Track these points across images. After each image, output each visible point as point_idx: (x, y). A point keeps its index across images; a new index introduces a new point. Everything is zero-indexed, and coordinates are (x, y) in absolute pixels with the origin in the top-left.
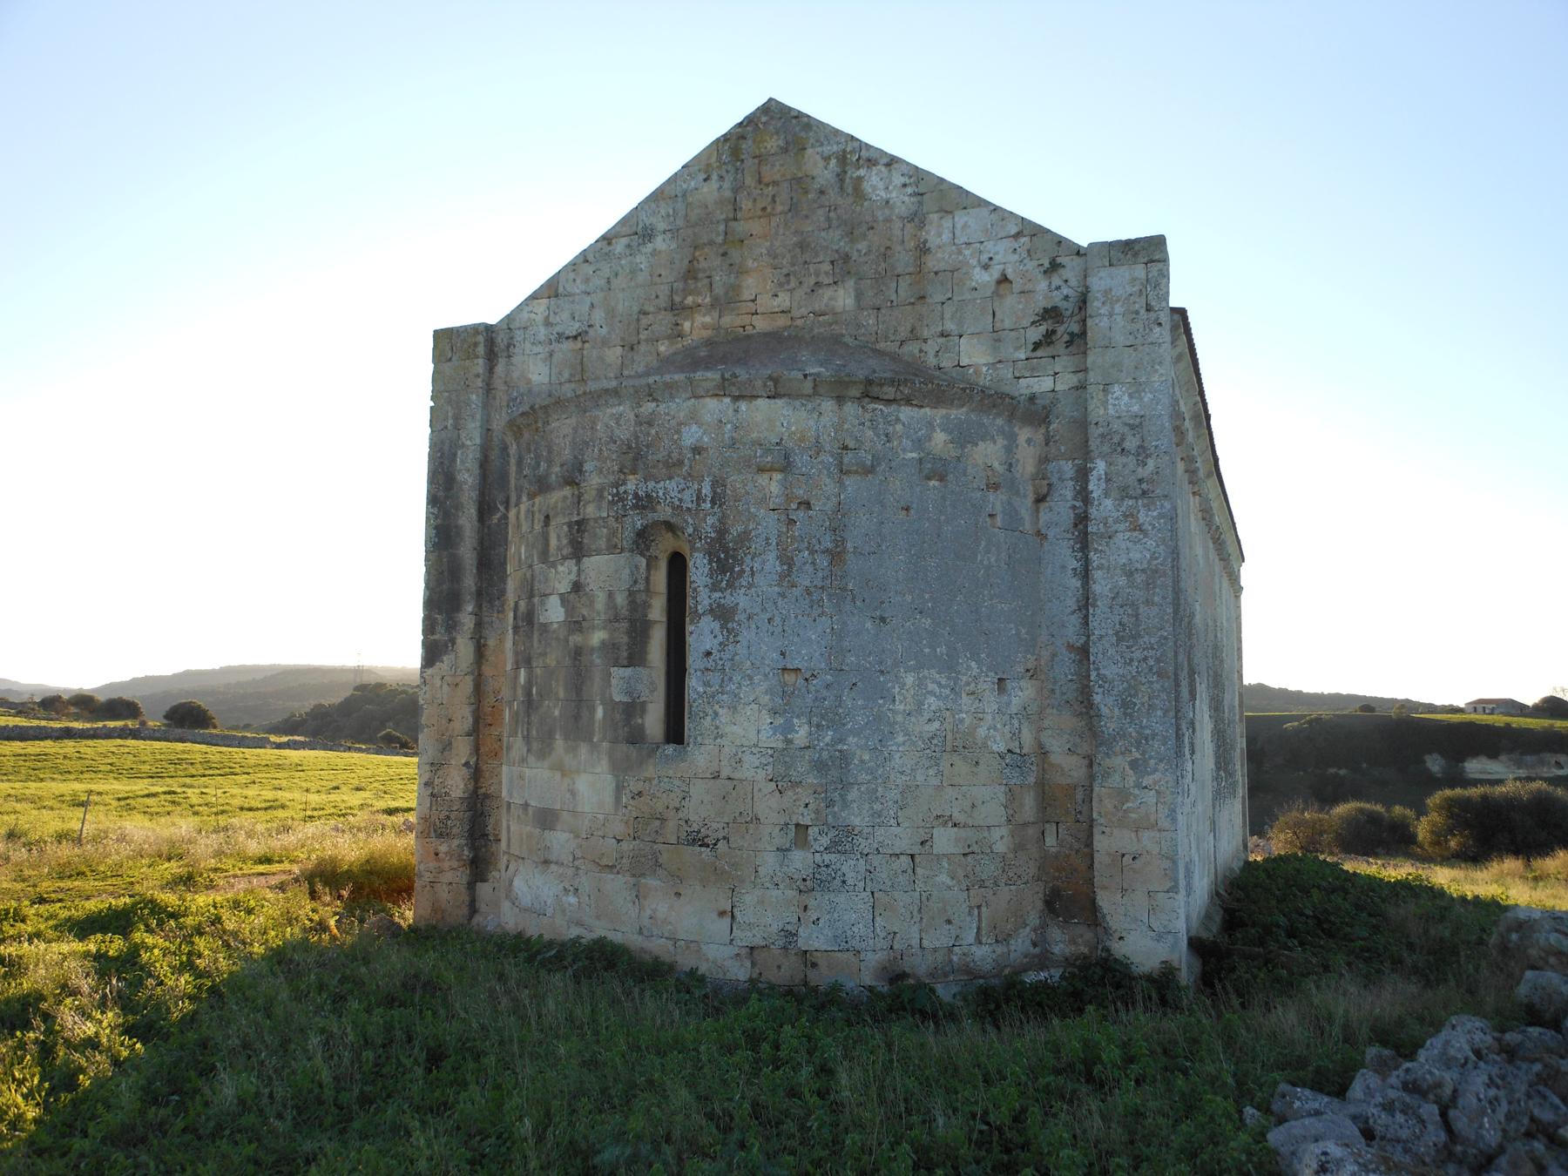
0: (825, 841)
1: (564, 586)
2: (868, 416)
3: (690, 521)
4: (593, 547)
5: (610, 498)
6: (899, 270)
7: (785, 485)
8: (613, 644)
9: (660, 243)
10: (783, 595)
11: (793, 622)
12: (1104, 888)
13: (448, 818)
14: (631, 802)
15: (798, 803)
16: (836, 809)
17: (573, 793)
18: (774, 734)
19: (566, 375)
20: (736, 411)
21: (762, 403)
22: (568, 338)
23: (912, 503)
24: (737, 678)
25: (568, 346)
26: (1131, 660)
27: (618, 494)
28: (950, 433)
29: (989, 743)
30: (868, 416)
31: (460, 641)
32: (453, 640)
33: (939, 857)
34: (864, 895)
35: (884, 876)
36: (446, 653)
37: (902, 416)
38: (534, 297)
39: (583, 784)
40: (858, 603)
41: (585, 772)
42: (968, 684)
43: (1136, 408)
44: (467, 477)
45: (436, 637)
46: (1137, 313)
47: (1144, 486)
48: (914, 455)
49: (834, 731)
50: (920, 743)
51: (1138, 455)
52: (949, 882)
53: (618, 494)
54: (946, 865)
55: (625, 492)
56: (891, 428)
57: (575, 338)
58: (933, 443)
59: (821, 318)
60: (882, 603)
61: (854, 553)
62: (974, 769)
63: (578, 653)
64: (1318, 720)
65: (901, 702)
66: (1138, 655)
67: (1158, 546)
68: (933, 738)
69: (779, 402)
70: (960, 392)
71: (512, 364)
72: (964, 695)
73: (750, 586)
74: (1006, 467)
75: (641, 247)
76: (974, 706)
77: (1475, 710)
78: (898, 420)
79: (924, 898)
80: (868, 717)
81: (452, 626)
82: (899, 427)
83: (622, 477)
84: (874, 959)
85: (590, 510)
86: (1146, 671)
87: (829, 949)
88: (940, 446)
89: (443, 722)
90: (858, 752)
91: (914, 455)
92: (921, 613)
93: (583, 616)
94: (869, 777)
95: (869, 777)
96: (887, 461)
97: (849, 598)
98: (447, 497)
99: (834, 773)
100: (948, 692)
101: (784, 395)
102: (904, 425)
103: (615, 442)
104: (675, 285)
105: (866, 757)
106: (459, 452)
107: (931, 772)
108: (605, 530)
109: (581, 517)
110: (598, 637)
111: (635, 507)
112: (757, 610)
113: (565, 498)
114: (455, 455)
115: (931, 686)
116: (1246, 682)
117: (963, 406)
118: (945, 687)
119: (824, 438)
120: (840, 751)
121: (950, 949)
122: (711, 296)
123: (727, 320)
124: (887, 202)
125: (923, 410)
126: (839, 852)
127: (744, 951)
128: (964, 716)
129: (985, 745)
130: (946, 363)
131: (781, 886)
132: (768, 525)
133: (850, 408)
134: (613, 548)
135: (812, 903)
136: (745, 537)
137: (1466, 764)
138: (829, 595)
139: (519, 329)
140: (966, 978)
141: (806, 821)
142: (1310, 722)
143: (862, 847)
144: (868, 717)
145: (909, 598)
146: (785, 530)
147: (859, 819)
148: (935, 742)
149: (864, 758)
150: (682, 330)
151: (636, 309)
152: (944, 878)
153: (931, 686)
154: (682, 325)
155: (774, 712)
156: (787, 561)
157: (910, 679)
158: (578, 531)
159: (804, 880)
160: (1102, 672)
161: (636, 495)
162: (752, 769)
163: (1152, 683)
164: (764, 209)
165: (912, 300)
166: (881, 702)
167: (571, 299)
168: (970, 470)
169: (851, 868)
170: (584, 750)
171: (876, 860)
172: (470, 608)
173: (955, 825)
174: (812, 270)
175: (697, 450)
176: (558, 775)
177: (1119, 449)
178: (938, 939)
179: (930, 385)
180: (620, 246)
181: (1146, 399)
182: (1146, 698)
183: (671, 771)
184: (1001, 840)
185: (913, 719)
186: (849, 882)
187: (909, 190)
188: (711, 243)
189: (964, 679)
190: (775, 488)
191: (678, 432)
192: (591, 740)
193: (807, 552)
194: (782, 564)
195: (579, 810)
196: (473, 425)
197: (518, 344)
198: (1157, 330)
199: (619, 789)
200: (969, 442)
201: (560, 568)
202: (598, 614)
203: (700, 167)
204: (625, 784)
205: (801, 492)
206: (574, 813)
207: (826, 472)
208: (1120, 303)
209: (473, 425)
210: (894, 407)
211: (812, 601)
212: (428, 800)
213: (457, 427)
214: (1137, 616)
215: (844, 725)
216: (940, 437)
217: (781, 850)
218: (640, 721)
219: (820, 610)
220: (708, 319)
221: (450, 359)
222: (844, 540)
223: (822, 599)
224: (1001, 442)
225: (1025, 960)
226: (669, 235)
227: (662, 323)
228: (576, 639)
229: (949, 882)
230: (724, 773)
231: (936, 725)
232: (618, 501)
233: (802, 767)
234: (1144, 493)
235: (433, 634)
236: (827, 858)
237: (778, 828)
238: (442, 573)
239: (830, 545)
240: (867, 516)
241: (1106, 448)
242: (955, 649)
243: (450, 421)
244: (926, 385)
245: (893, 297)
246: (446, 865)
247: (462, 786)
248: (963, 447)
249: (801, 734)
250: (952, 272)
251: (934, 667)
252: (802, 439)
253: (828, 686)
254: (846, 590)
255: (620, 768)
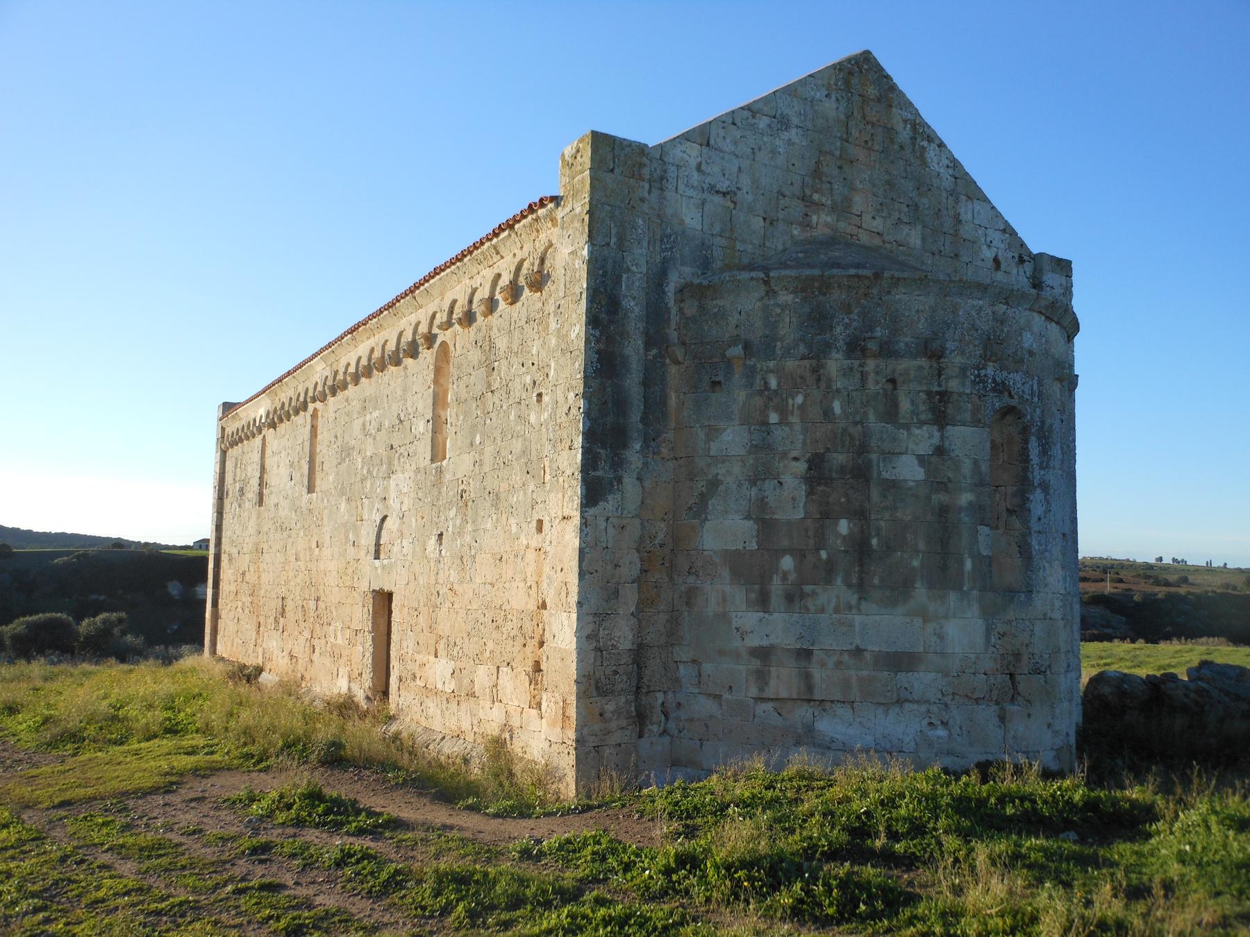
1: (924, 448)
4: (958, 418)
5: (972, 377)
6: (945, 230)
8: (980, 506)
9: (793, 134)
13: (616, 672)
14: (998, 641)
17: (941, 637)
19: (717, 229)
22: (717, 192)
25: (718, 199)
27: (979, 376)
31: (626, 480)
32: (620, 480)
36: (611, 492)
39: (952, 629)
41: (954, 617)
44: (633, 304)
45: (600, 473)
53: (979, 376)
55: (985, 376)
57: (724, 194)
59: (901, 248)
63: (943, 511)
64: (85, 555)
71: (665, 198)
75: (780, 132)
77: (200, 547)
81: (618, 463)
83: (983, 362)
85: (954, 385)
89: (609, 567)
93: (949, 478)
98: (611, 322)
103: (977, 330)
104: (806, 178)
106: (625, 276)
108: (970, 405)
109: (943, 388)
110: (965, 498)
111: (994, 390)
113: (920, 368)
114: (619, 277)
116: (1080, 556)
122: (832, 200)
123: (842, 225)
124: (939, 175)
134: (976, 422)
137: (197, 588)
139: (673, 165)
142: (78, 557)
150: (811, 221)
151: (775, 188)
154: (811, 217)
158: (940, 401)
161: (994, 380)
164: (866, 142)
165: (952, 255)
167: (721, 155)
170: (953, 597)
172: (638, 447)
174: (896, 207)
176: (918, 621)
183: (1024, 614)
188: (831, 153)
191: (1021, 335)
192: (961, 589)
195: (950, 651)
196: (640, 251)
197: (671, 180)
199: (988, 631)
201: (917, 431)
202: (965, 477)
204: (994, 627)
206: (943, 654)
209: (640, 251)
212: (592, 655)
213: (621, 247)
220: (829, 219)
221: (612, 171)
226: (800, 131)
227: (797, 209)
228: (939, 498)
232: (979, 383)
235: (595, 469)
238: (605, 403)
243: (614, 240)
245: (942, 249)
246: (613, 725)
247: (630, 637)
255: (989, 613)
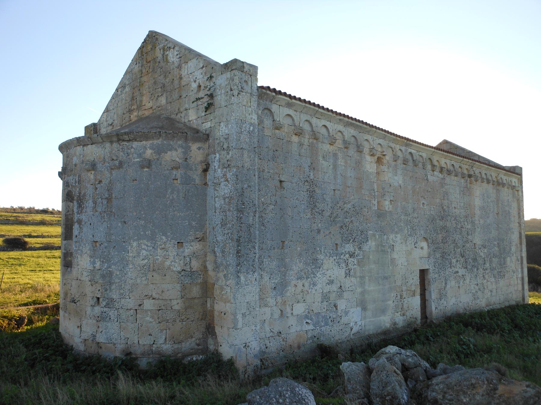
0: (104, 303)
2: (121, 147)
3: (74, 190)
7: (95, 175)
10: (93, 215)
11: (96, 224)
12: (217, 325)
15: (96, 290)
16: (108, 292)
18: (91, 265)
20: (83, 150)
21: (89, 146)
23: (136, 178)
24: (82, 245)
26: (225, 234)
28: (154, 150)
29: (171, 267)
30: (121, 147)
33: (146, 311)
34: (116, 323)
35: (124, 317)
37: (134, 146)
38: (104, 113)
40: (116, 217)
42: (161, 245)
43: (227, 131)
46: (228, 92)
47: (229, 163)
48: (138, 160)
49: (108, 263)
50: (139, 268)
51: (227, 150)
52: (151, 320)
54: (150, 314)
56: (129, 151)
58: (146, 154)
60: (125, 216)
61: (115, 198)
62: (164, 278)
65: (131, 253)
66: (226, 232)
67: (232, 187)
68: (144, 266)
69: (94, 145)
70: (154, 134)
72: (159, 250)
73: (86, 212)
74: (184, 160)
76: (164, 253)
78: (132, 147)
79: (139, 326)
80: (119, 258)
82: (132, 150)
84: (120, 347)
86: (228, 238)
87: (105, 342)
88: (149, 155)
90: (115, 272)
91: (138, 160)
92: (140, 219)
94: (119, 281)
95: (119, 281)
96: (127, 163)
97: (113, 215)
99: (107, 279)
100: (151, 248)
101: (95, 143)
102: (134, 149)
105: (118, 273)
107: (143, 279)
112: (87, 221)
115: (143, 247)
117: (159, 139)
118: (149, 246)
119: (106, 157)
120: (109, 271)
121: (151, 345)
125: (142, 142)
126: (109, 308)
127: (83, 341)
128: (159, 257)
129: (169, 268)
130: (186, 121)
131: (92, 319)
132: (89, 190)
133: (115, 145)
135: (100, 325)
136: (85, 195)
138: (107, 214)
140: (158, 356)
141: (99, 296)
143: (116, 306)
144: (119, 258)
145: (135, 214)
146: (94, 191)
147: (115, 296)
148: (145, 267)
149: (117, 273)
152: (148, 318)
153: (143, 247)
155: (91, 257)
156: (95, 203)
157: (135, 244)
159: (98, 317)
160: (217, 239)
162: (85, 278)
163: (230, 243)
166: (123, 253)
168: (163, 162)
169: (112, 313)
171: (121, 311)
173: (154, 299)
175: (76, 165)
177: (222, 148)
178: (146, 341)
179: (140, 133)
180: (120, 90)
181: (229, 127)
182: (228, 249)
184: (177, 304)
185: (136, 259)
186: (112, 318)
187: (178, 57)
189: (159, 243)
190: (92, 177)
193: (100, 199)
194: (93, 204)
198: (233, 98)
200: (163, 152)
203: (135, 61)
205: (99, 177)
207: (106, 169)
208: (223, 89)
210: (131, 142)
211: (102, 217)
214: (226, 216)
215: (111, 261)
216: (149, 152)
217: (92, 306)
218: (70, 259)
219: (104, 220)
222: (112, 193)
223: (104, 216)
224: (180, 150)
225: (191, 351)
229: (151, 320)
230: (79, 278)
231: (146, 261)
233: (98, 277)
234: (229, 166)
236: (105, 309)
237: (91, 298)
239: (107, 196)
240: (120, 184)
241: (219, 149)
242: (155, 232)
244: (139, 133)
248: (159, 154)
249: (98, 265)
250: (187, 85)
251: (145, 239)
252: (100, 158)
253: (106, 248)
254: (112, 212)
